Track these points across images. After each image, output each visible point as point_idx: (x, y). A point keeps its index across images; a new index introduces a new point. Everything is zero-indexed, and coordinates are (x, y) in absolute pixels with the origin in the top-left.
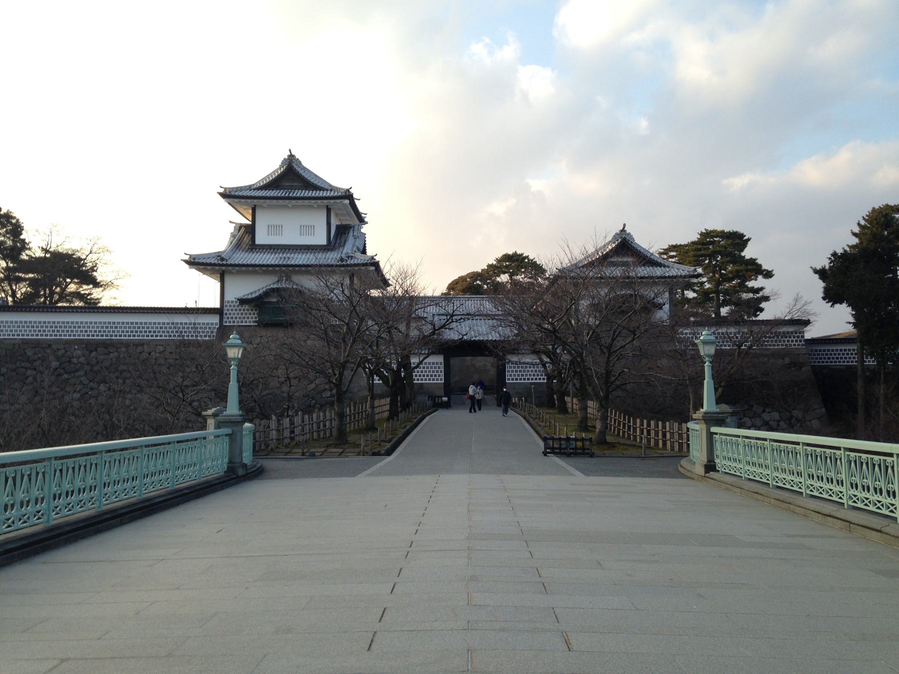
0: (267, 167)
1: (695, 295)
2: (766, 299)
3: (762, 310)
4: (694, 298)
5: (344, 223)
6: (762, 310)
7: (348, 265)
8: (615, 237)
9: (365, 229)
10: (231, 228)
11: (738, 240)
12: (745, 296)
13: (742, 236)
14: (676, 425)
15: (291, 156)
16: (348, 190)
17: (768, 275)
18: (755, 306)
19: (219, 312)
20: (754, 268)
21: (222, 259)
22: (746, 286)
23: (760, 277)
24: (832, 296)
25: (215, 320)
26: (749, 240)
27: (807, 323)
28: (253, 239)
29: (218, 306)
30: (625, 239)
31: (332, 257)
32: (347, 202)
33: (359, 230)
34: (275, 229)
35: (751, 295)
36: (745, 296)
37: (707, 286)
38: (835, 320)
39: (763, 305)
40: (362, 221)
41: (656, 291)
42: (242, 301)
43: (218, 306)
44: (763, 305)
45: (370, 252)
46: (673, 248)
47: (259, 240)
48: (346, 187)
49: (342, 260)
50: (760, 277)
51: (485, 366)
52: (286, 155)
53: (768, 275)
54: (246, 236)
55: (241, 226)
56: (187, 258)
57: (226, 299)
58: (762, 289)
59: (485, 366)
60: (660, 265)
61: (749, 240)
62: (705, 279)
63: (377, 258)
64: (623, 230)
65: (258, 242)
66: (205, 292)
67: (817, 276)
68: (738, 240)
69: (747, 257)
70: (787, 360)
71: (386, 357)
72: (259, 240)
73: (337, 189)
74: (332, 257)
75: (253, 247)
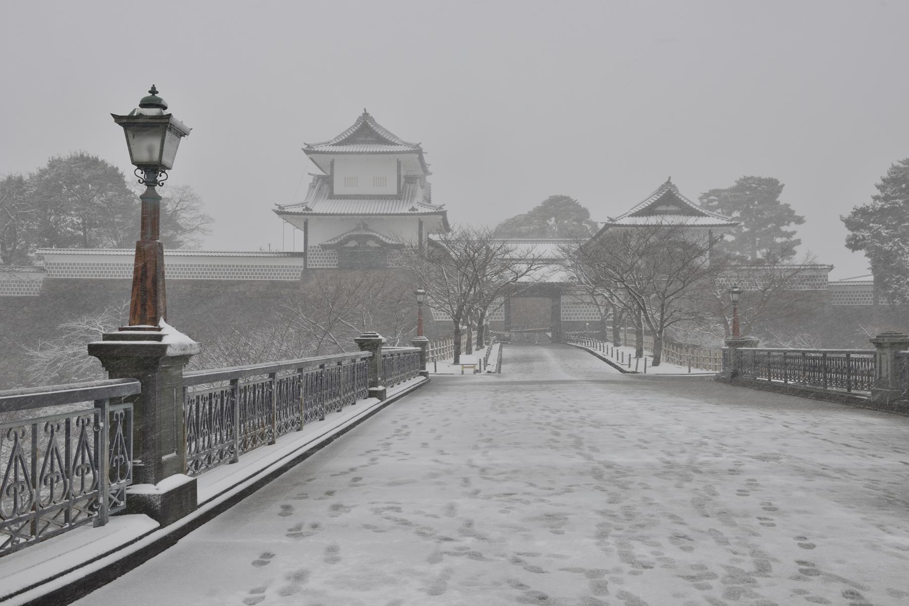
0: (348, 122)
2: (798, 242)
4: (733, 242)
7: (418, 214)
8: (662, 188)
9: (429, 179)
10: (310, 179)
11: (772, 187)
13: (777, 182)
14: (189, 372)
15: (366, 114)
16: (418, 145)
17: (800, 221)
19: (303, 255)
20: (788, 215)
21: (307, 209)
22: (780, 230)
23: (792, 224)
24: (854, 244)
25: (299, 262)
26: (783, 186)
28: (332, 188)
29: (302, 250)
30: (670, 192)
32: (441, 217)
33: (425, 179)
35: (784, 239)
36: (779, 240)
37: (745, 230)
38: (853, 269)
39: (795, 248)
40: (426, 172)
42: (324, 247)
43: (302, 250)
44: (795, 248)
45: (436, 201)
46: (714, 192)
48: (416, 142)
50: (792, 224)
52: (360, 113)
53: (800, 221)
54: (324, 184)
55: (319, 177)
56: (276, 208)
57: (309, 244)
58: (794, 233)
60: (703, 215)
61: (783, 186)
63: (445, 208)
64: (668, 182)
66: (291, 239)
67: (843, 224)
68: (772, 187)
69: (782, 203)
73: (406, 144)
75: (332, 196)
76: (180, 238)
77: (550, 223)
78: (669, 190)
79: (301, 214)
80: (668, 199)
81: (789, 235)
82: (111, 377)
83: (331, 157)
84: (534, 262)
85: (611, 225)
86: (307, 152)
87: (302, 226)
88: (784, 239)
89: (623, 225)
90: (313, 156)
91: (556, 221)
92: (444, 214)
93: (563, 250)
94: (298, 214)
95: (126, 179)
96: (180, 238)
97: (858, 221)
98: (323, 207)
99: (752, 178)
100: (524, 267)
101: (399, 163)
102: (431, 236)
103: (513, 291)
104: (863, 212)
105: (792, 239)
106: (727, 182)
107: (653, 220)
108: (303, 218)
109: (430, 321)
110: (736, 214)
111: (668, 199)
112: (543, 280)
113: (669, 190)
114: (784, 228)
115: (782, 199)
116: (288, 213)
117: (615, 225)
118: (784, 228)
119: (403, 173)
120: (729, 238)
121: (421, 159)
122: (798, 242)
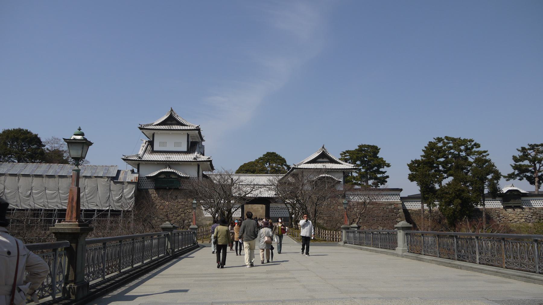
1: (357, 175)
2: (388, 177)
3: (386, 182)
4: (357, 176)
5: (194, 140)
6: (386, 182)
9: (203, 143)
11: (375, 150)
12: (379, 176)
15: (172, 110)
17: (388, 166)
18: (383, 181)
20: (382, 163)
24: (412, 178)
26: (380, 149)
27: (401, 190)
31: (190, 157)
34: (163, 144)
36: (379, 176)
37: (363, 170)
39: (387, 180)
40: (202, 140)
41: (58, 291)
47: (155, 149)
49: (195, 159)
50: (385, 167)
51: (258, 208)
53: (388, 166)
59: (258, 208)
61: (380, 149)
62: (361, 167)
65: (155, 149)
69: (380, 157)
70: (393, 206)
71: (17, 142)
72: (155, 149)
74: (190, 157)
75: (153, 152)
76: (425, 149)
77: (266, 166)
78: (324, 151)
79: (136, 160)
80: (324, 157)
81: (384, 173)
82: (57, 240)
83: (153, 132)
84: (255, 186)
85: (296, 168)
86: (141, 129)
87: (137, 167)
88: (381, 175)
89: (301, 168)
90: (144, 131)
91: (269, 164)
92: (211, 161)
93: (270, 180)
94: (135, 160)
95: (42, 140)
96: (425, 149)
97: (414, 166)
98: (148, 157)
99: (365, 145)
100: (249, 189)
101: (188, 135)
102: (204, 173)
103: (245, 201)
104: (416, 161)
105: (385, 175)
106: (354, 147)
107: (319, 166)
108: (139, 163)
109: (203, 217)
110: (358, 163)
111: (324, 157)
112: (259, 195)
113: (324, 151)
114: (381, 170)
115: (379, 155)
116: (129, 160)
117: (297, 168)
118: (381, 170)
119: (190, 140)
120: (355, 174)
121: (200, 133)
122: (388, 177)
